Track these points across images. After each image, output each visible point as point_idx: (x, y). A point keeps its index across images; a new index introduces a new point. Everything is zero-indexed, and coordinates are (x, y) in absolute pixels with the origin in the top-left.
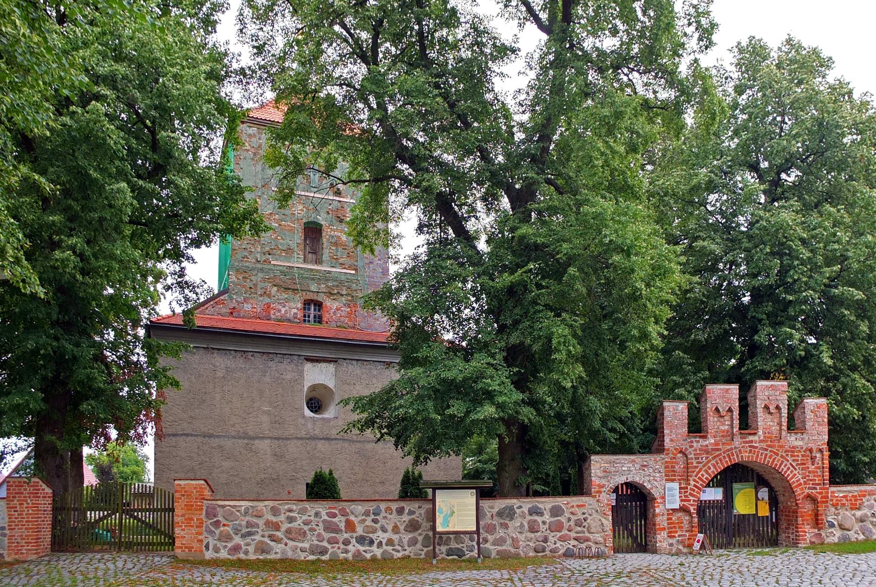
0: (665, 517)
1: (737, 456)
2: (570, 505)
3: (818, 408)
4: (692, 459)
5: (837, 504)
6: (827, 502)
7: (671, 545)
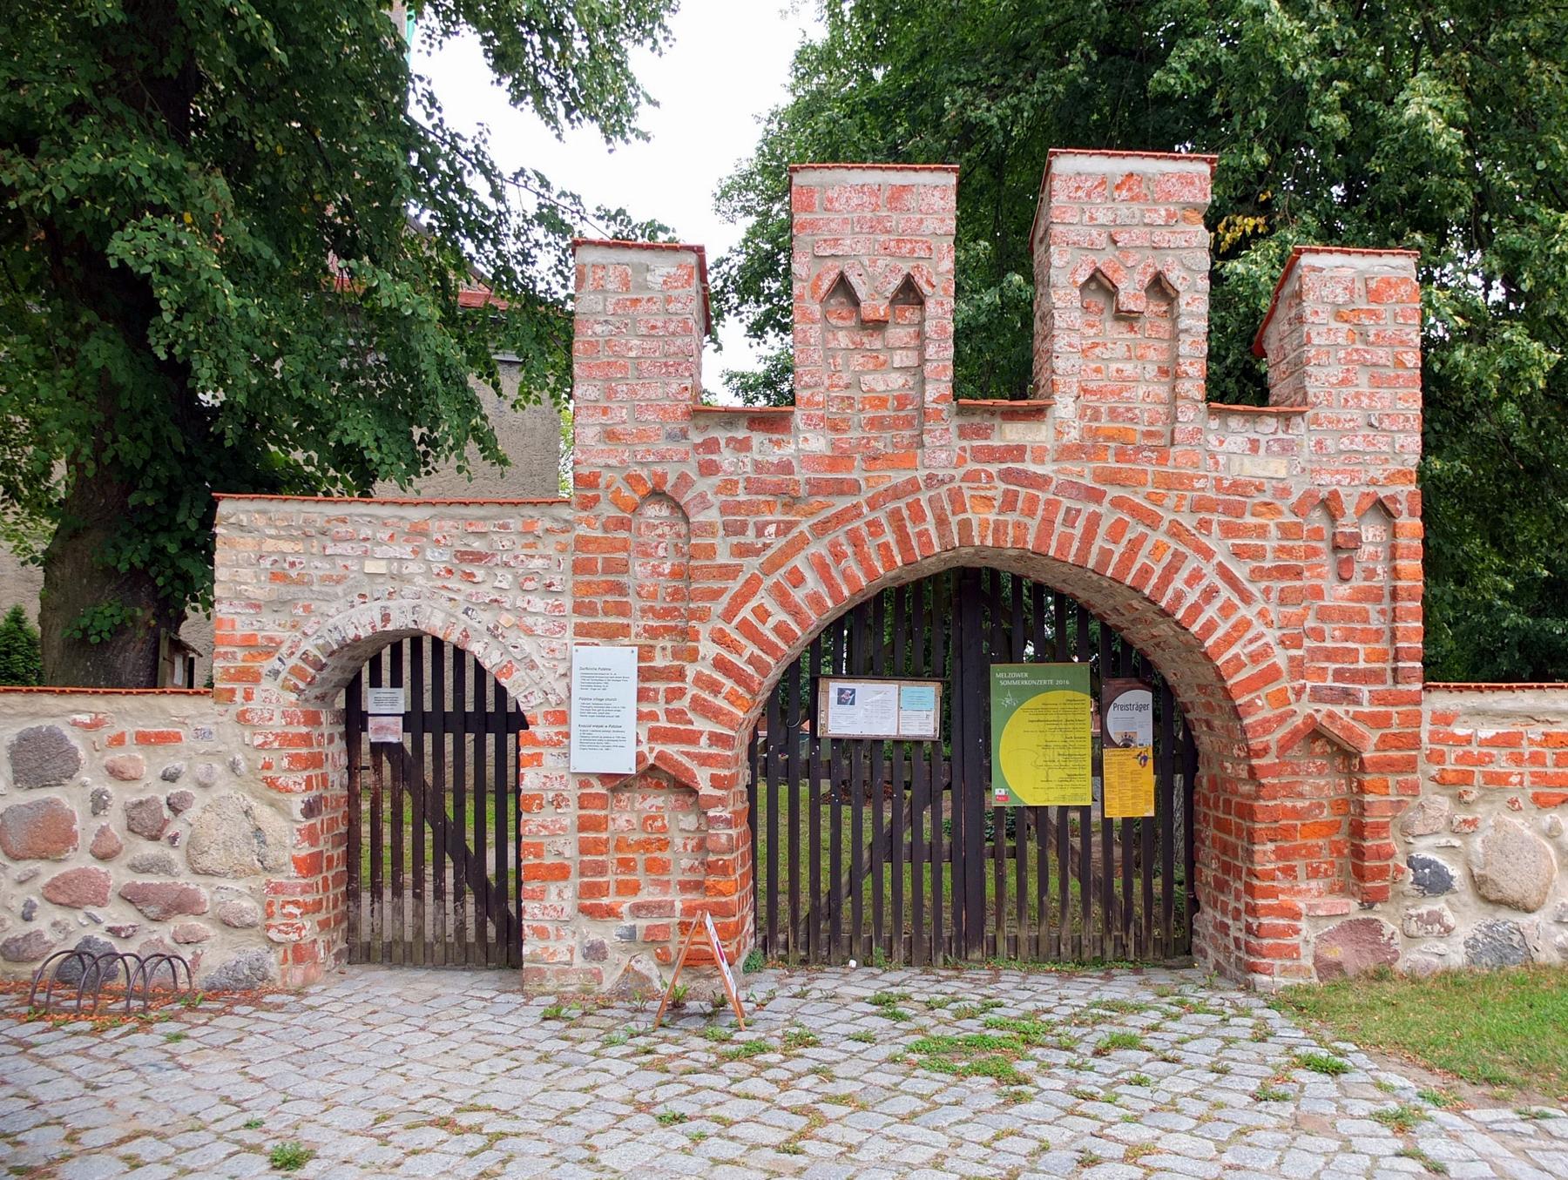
0: (570, 815)
1: (942, 522)
2: (106, 733)
3: (1374, 295)
4: (708, 529)
5: (1466, 779)
6: (1410, 765)
7: (595, 952)
